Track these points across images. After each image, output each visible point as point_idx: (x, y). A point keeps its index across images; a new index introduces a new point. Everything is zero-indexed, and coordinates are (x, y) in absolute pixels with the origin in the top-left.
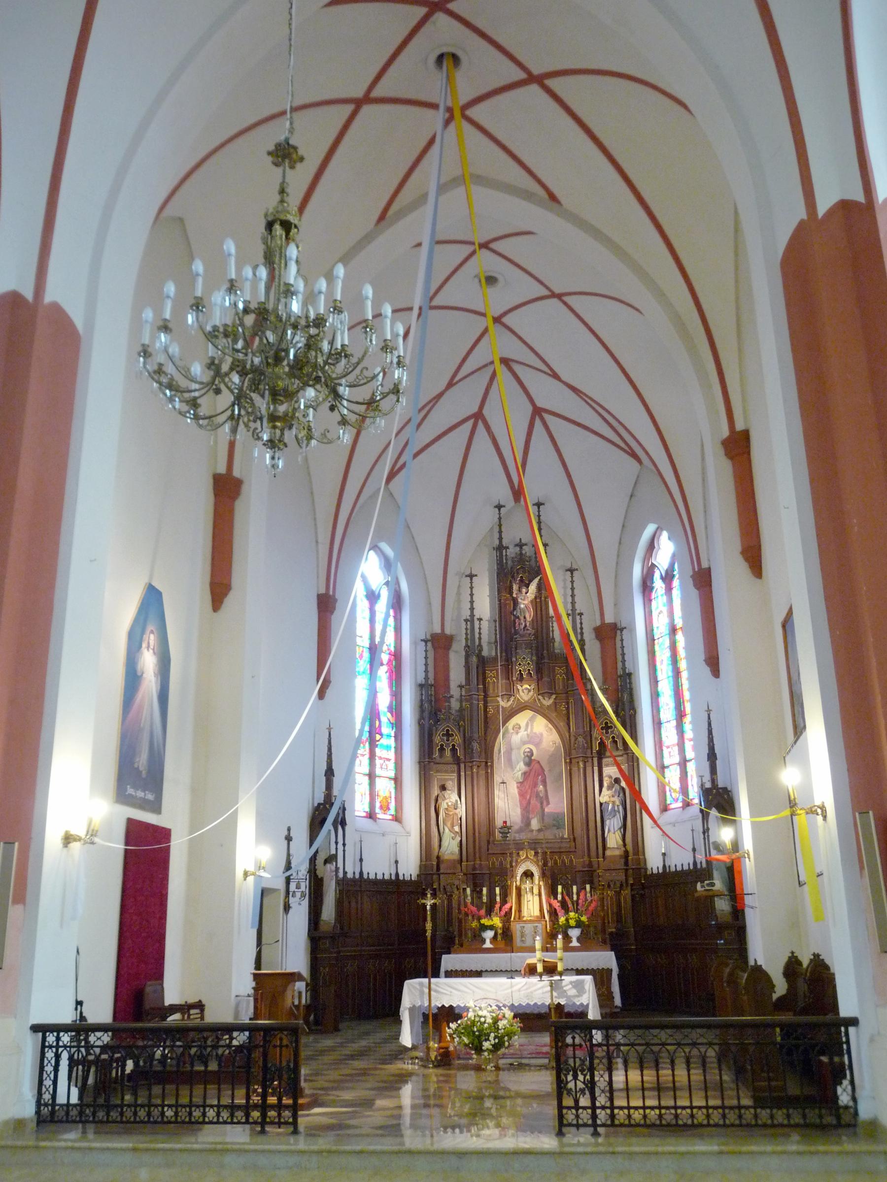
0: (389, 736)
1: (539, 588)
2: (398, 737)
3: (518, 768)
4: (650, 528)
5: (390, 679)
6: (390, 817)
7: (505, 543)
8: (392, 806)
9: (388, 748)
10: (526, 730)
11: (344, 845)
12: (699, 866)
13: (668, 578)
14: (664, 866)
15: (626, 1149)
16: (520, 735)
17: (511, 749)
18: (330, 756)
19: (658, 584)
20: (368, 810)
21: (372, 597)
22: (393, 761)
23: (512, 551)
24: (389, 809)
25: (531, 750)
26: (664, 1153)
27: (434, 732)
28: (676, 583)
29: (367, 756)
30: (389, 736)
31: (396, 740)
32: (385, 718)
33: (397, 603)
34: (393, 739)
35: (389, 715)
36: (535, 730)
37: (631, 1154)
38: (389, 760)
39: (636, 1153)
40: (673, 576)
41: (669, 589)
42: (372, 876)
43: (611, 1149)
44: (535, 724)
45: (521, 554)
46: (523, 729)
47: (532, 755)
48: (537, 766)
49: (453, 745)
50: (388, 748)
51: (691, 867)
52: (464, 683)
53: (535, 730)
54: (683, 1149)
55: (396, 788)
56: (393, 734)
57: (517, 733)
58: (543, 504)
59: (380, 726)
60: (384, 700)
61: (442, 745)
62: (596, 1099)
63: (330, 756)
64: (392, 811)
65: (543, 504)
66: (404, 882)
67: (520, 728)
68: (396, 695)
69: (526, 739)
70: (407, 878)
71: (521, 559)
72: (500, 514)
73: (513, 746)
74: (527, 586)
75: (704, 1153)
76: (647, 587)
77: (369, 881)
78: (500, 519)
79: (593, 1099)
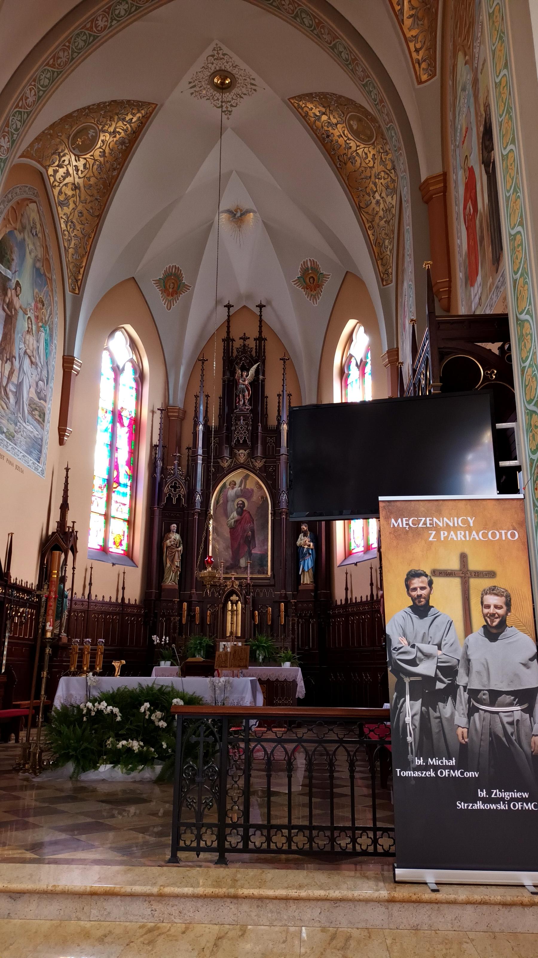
0: (125, 486)
1: (257, 371)
2: (134, 488)
3: (232, 516)
4: (351, 323)
5: (130, 439)
6: (122, 552)
7: (232, 335)
8: (125, 543)
9: (124, 494)
10: (240, 486)
11: (74, 568)
12: (375, 598)
13: (361, 366)
14: (346, 599)
15: (256, 892)
16: (235, 489)
17: (227, 501)
18: (66, 490)
19: (354, 372)
20: (102, 544)
21: (117, 371)
22: (128, 506)
23: (238, 344)
24: (121, 544)
25: (243, 502)
26: (308, 899)
27: (164, 483)
28: (368, 369)
29: (105, 499)
30: (125, 486)
31: (131, 489)
32: (124, 469)
33: (140, 378)
34: (129, 488)
35: (127, 469)
36: (247, 487)
37: (261, 898)
38: (125, 505)
39: (268, 898)
40: (366, 363)
41: (363, 374)
42: (100, 598)
43: (232, 891)
44: (248, 482)
45: (244, 345)
46: (237, 486)
47: (244, 506)
48: (247, 515)
49: (180, 496)
50: (124, 494)
51: (369, 599)
52: (191, 446)
53: (247, 487)
54: (336, 894)
55: (129, 528)
56: (129, 484)
57: (233, 488)
58: (265, 306)
59: (118, 476)
60: (123, 455)
61: (170, 495)
62: (226, 814)
63: (66, 490)
64: (124, 547)
65: (265, 306)
66: (129, 605)
67: (235, 484)
68: (134, 453)
69: (240, 493)
70: (132, 602)
71: (244, 349)
72: (229, 312)
73: (229, 498)
74: (248, 370)
75: (367, 901)
76: (343, 374)
77: (97, 603)
78: (229, 316)
79: (223, 813)
